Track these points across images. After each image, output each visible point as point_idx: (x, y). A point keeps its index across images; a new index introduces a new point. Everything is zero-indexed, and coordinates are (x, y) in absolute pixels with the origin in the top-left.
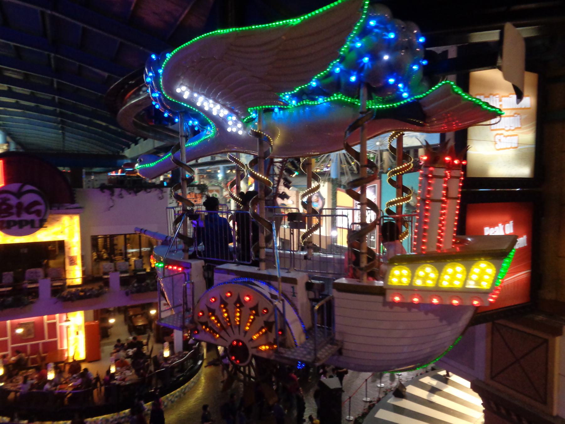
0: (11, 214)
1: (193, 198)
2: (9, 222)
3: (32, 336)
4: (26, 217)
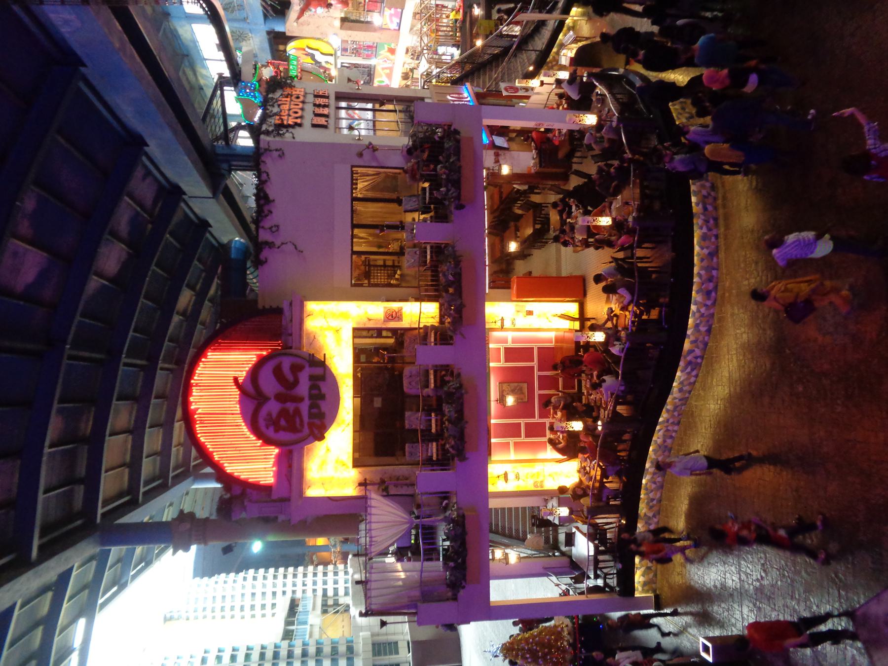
0: (297, 412)
1: (291, 100)
2: (311, 416)
3: (525, 385)
4: (303, 388)
